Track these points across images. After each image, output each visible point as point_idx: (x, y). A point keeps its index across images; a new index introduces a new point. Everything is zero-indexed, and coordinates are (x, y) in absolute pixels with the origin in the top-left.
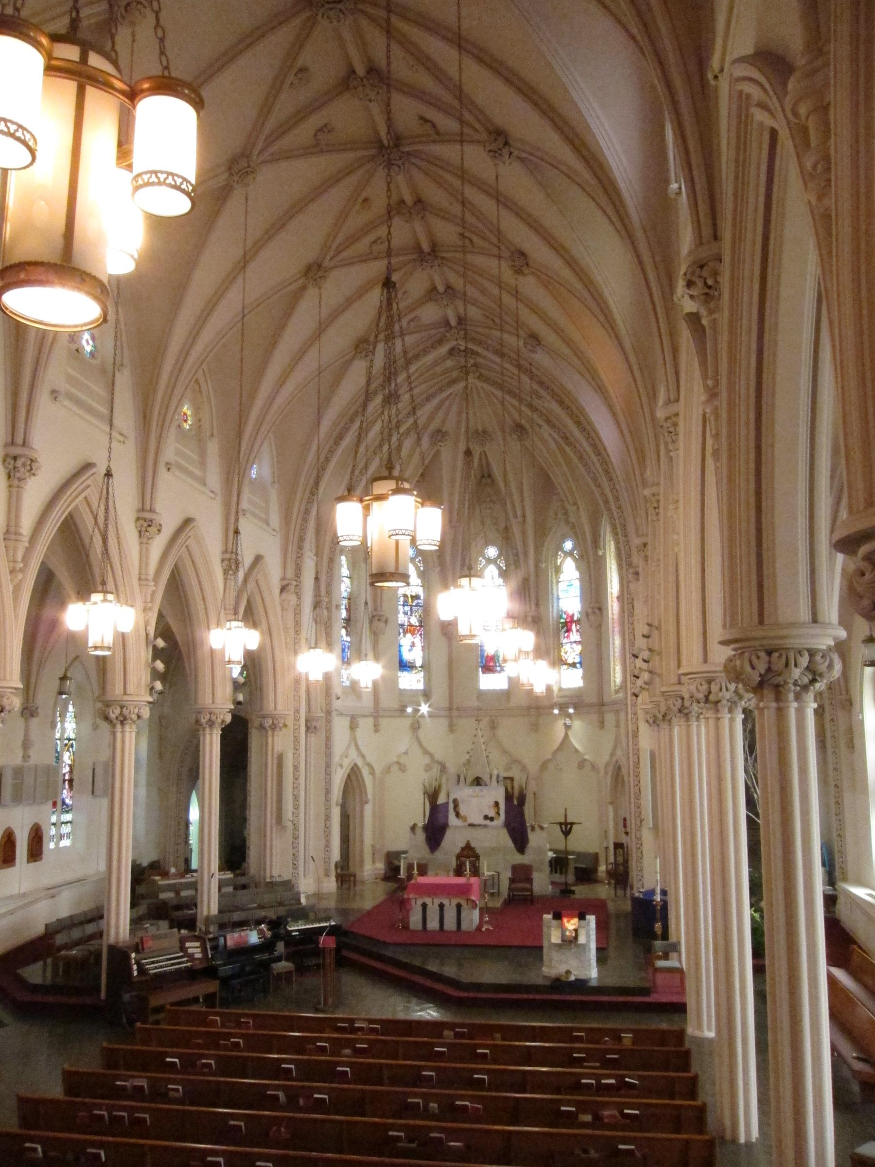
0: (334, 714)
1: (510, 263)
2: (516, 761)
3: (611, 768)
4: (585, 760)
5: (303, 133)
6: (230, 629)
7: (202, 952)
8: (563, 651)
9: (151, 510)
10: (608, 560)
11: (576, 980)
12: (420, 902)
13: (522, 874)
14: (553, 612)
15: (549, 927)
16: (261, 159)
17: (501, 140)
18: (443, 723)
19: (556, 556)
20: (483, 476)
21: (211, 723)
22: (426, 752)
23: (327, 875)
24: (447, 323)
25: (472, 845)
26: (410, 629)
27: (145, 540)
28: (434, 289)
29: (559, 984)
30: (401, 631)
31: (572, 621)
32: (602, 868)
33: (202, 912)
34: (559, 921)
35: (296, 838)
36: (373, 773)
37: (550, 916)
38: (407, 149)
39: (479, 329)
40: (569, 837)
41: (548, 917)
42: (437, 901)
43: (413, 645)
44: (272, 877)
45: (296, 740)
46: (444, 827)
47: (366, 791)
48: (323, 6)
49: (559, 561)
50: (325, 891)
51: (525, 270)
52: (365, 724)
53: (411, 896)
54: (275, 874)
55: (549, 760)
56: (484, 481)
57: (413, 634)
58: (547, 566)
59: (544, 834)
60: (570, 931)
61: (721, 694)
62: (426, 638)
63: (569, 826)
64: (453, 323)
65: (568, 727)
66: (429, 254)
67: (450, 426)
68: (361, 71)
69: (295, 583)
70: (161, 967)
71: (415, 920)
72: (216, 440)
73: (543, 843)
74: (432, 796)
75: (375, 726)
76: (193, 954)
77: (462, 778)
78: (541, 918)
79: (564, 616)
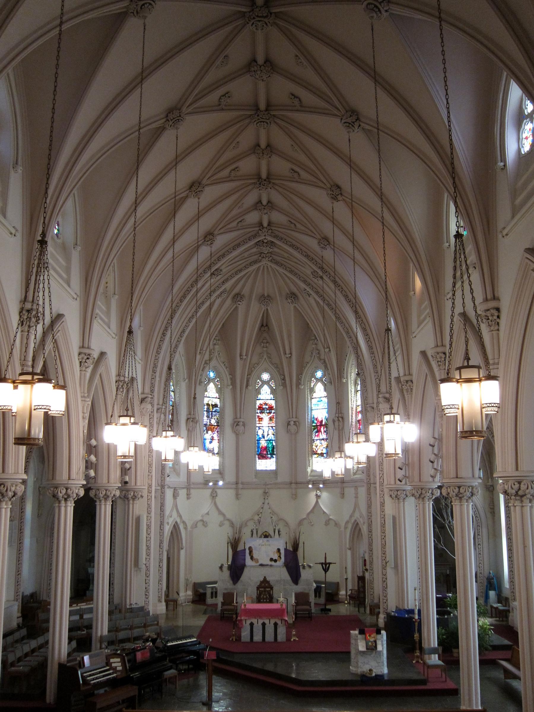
0: (166, 487)
1: (330, 192)
2: (281, 519)
3: (350, 526)
4: (330, 519)
5: (213, 98)
6: (166, 437)
7: (122, 665)
8: (314, 445)
9: (89, 348)
10: (349, 386)
11: (376, 675)
12: (248, 622)
13: (302, 598)
14: (308, 419)
15: (356, 640)
16: (190, 110)
17: (354, 118)
18: (231, 493)
19: (310, 381)
20: (262, 325)
21: (106, 497)
22: (220, 513)
23: (160, 601)
24: (261, 224)
25: (268, 579)
26: (209, 428)
27: (84, 368)
28: (260, 202)
29: (366, 679)
30: (205, 428)
31: (321, 425)
32: (342, 592)
33: (96, 633)
34: (364, 636)
35: (147, 576)
36: (186, 528)
37: (357, 632)
38: (273, 113)
39: (280, 229)
40: (327, 573)
41: (355, 633)
42: (261, 621)
43: (212, 439)
44: (131, 604)
45: (149, 506)
46: (243, 566)
47: (181, 539)
48: (254, 18)
49: (312, 384)
50: (158, 613)
51: (340, 198)
52: (183, 493)
53: (243, 618)
54: (133, 602)
55: (305, 519)
56: (263, 329)
57: (212, 431)
58: (304, 388)
59: (311, 571)
60: (372, 642)
61: (527, 491)
62: (221, 434)
63: (328, 565)
64: (265, 224)
65: (318, 497)
66: (265, 180)
67: (246, 291)
68: (261, 60)
69: (150, 396)
70: (97, 678)
71: (245, 634)
72: (116, 297)
73: (310, 576)
74: (234, 544)
75: (187, 495)
76: (116, 667)
77: (255, 532)
78: (350, 633)
79: (316, 422)
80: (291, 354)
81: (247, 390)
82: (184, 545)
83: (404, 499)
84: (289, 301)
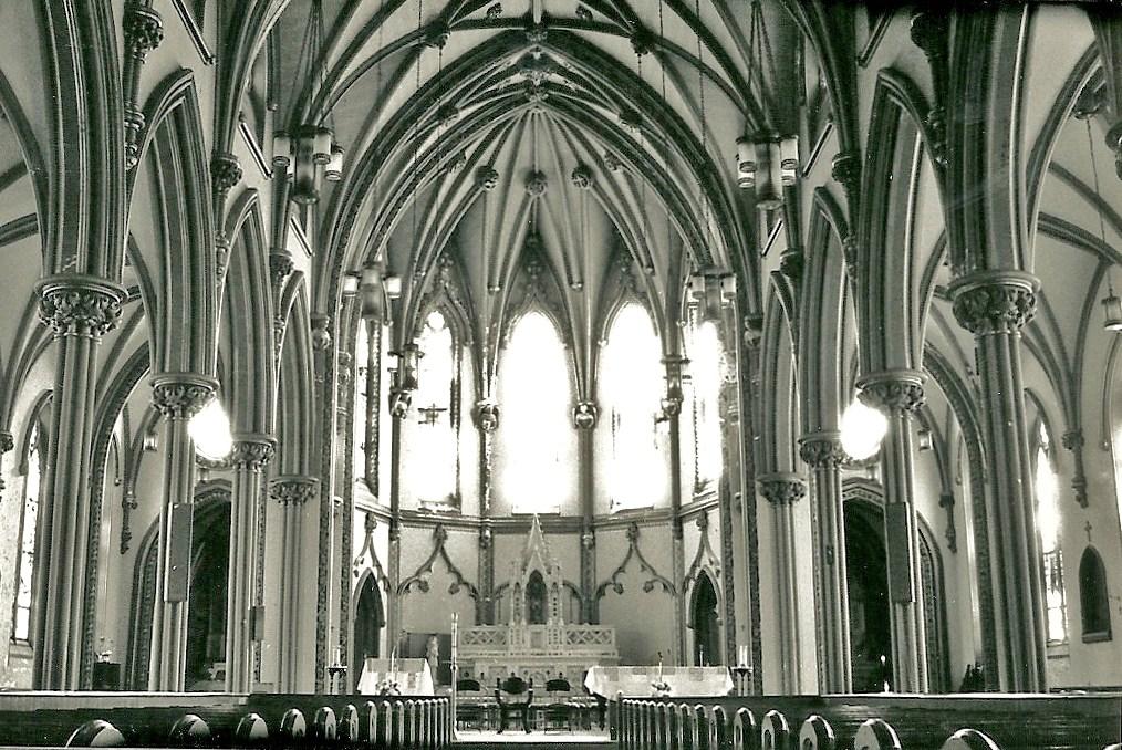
80: (582, 282)
81: (503, 351)
82: (386, 619)
83: (792, 499)
84: (580, 180)
